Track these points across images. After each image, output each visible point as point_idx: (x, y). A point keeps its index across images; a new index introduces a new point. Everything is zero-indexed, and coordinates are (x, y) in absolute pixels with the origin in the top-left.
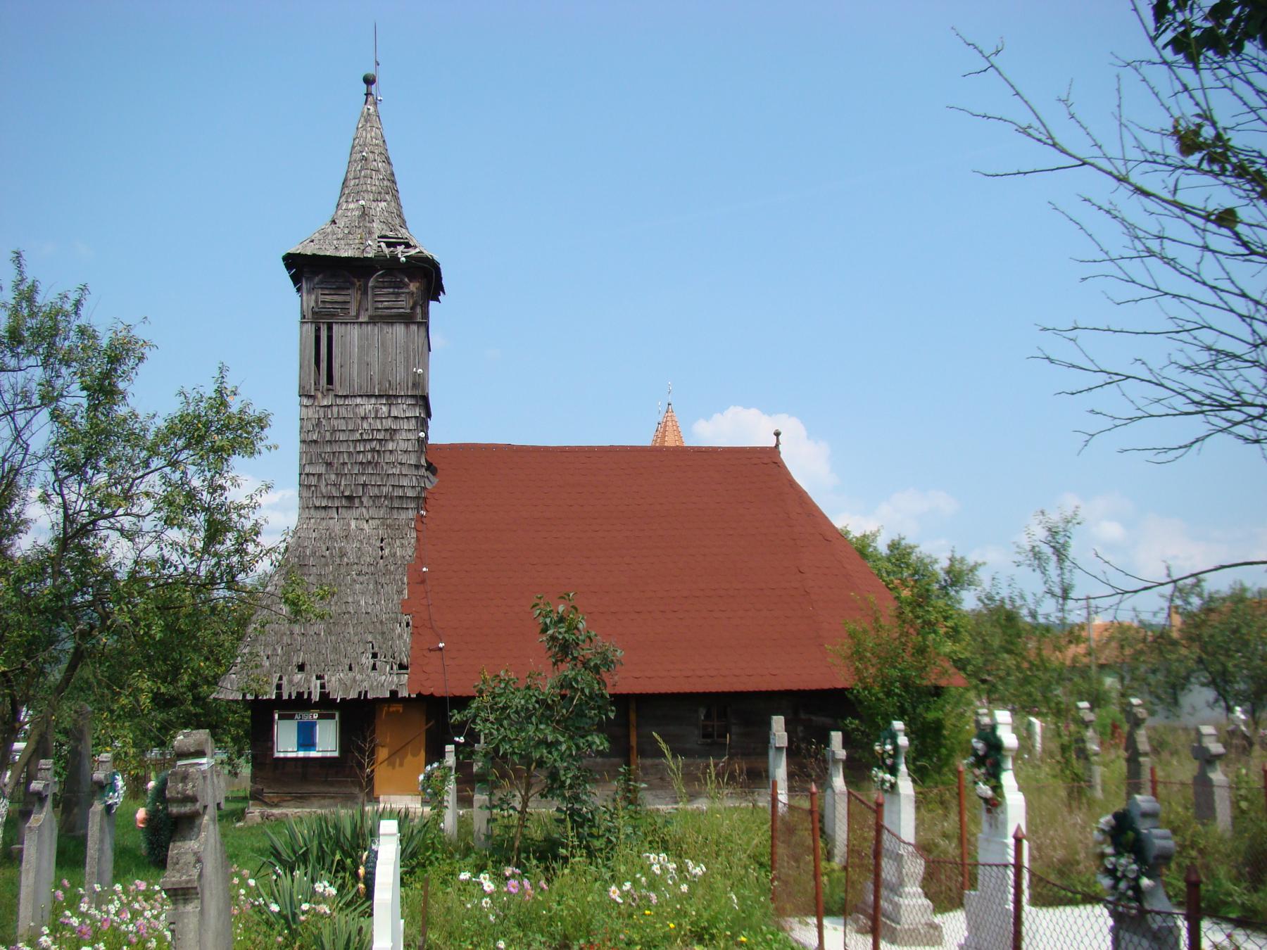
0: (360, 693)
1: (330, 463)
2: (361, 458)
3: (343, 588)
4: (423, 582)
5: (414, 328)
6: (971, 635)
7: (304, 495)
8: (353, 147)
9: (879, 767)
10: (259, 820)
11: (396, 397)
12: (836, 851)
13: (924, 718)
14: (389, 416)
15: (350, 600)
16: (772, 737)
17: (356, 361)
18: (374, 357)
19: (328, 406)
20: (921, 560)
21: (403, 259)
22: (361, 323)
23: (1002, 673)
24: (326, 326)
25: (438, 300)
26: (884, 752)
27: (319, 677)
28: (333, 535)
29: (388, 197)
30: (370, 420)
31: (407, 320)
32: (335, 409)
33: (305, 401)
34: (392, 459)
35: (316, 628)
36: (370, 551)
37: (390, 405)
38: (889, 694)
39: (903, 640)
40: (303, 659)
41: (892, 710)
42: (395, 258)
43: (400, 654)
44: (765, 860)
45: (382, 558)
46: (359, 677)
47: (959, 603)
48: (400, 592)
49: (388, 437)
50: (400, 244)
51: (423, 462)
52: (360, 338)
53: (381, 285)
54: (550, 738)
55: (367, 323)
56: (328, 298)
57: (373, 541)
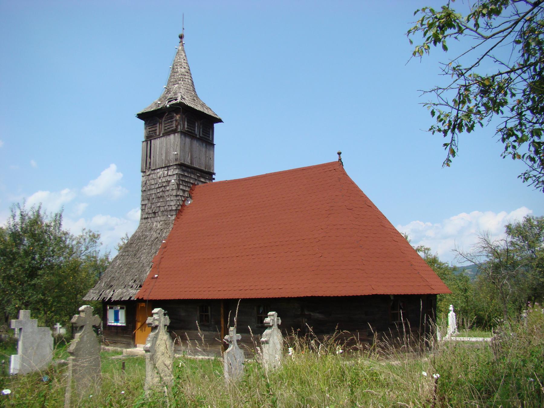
11: (170, 166)
30: (162, 178)
32: (151, 176)
56: (151, 130)
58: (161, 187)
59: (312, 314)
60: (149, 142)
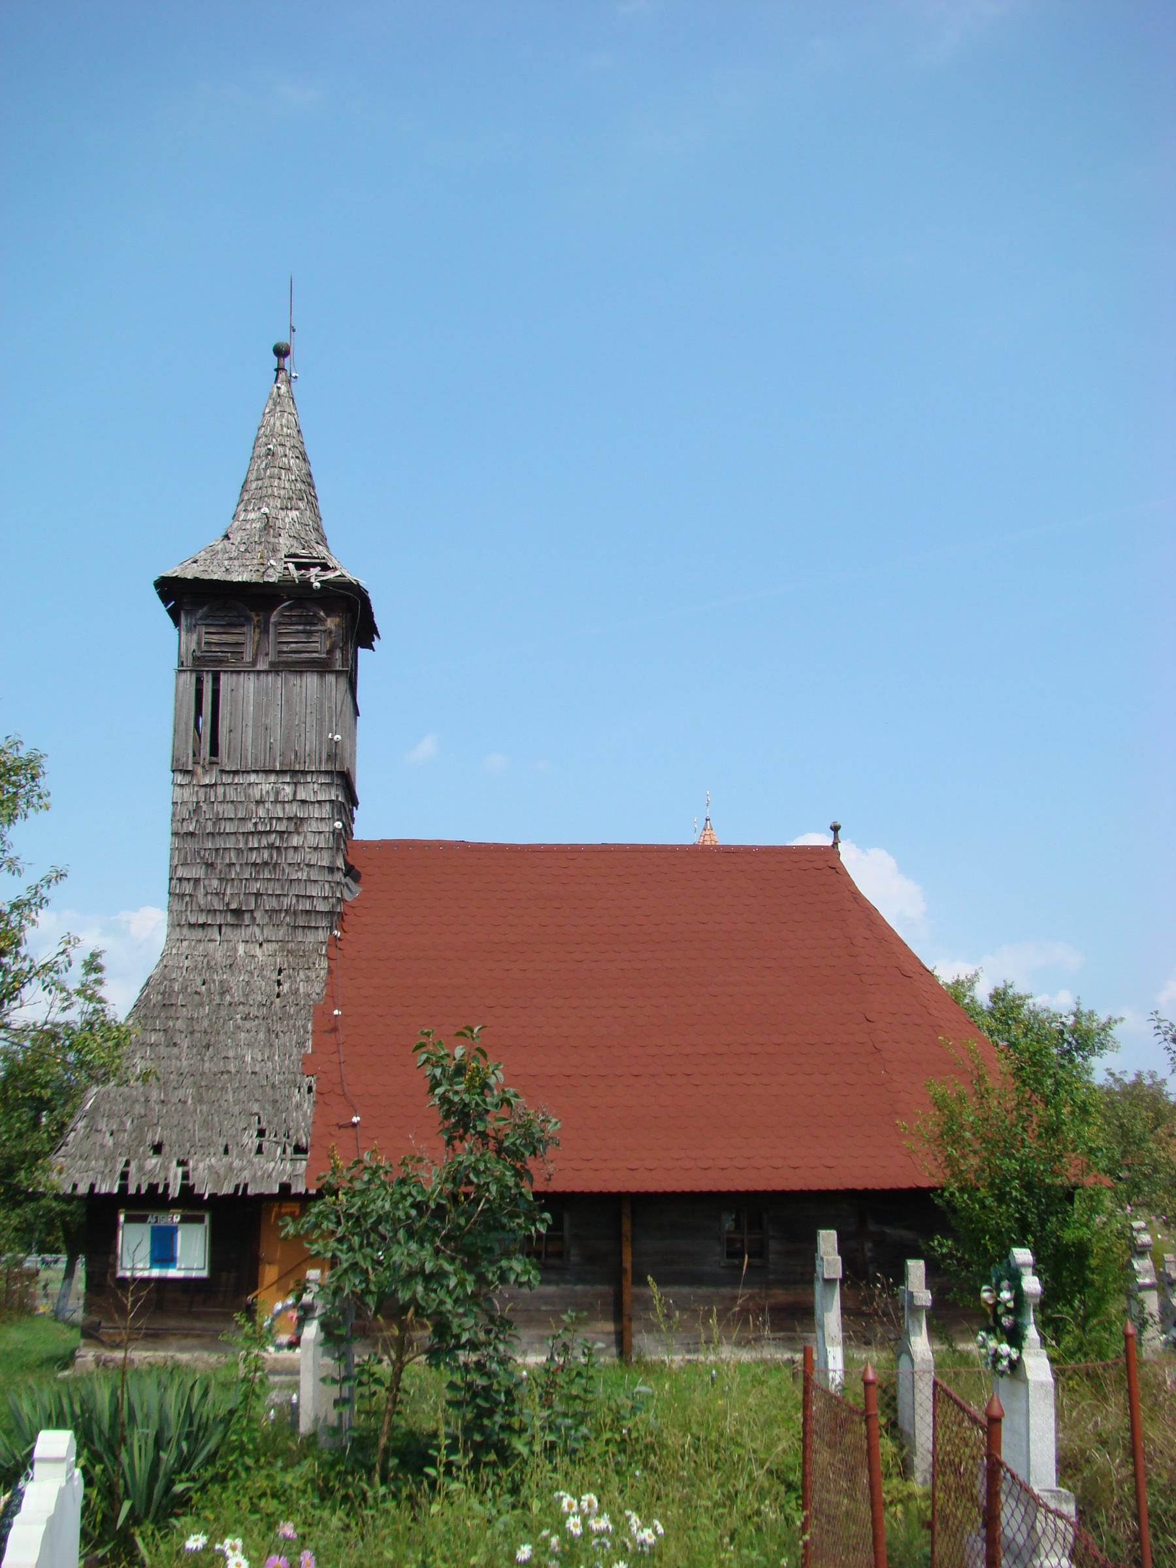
0: (237, 1187)
1: (212, 864)
2: (253, 857)
3: (222, 1037)
4: (334, 1030)
5: (331, 679)
6: (1104, 1116)
7: (175, 908)
8: (258, 438)
9: (989, 1330)
10: (92, 1366)
11: (304, 773)
12: (916, 1460)
13: (1058, 1238)
14: (294, 800)
15: (231, 1054)
16: (818, 1262)
17: (250, 723)
18: (276, 718)
19: (212, 786)
20: (1034, 1014)
21: (318, 585)
22: (259, 672)
23: (1147, 1170)
24: (210, 676)
25: (372, 648)
26: (998, 1303)
27: (181, 1163)
28: (213, 963)
29: (301, 505)
31: (321, 667)
32: (220, 790)
33: (180, 778)
35: (180, 1093)
36: (263, 986)
37: (296, 784)
38: (1001, 1198)
39: (1024, 1113)
40: (161, 1136)
41: (1007, 1224)
42: (307, 584)
43: (297, 1131)
44: (795, 1477)
45: (278, 996)
46: (237, 1163)
47: (1088, 1073)
48: (301, 1044)
49: (292, 828)
50: (314, 565)
51: (340, 863)
52: (257, 692)
53: (287, 620)
54: (429, 1267)
55: (267, 672)
56: (215, 638)
57: (267, 973)
59: (887, 1230)
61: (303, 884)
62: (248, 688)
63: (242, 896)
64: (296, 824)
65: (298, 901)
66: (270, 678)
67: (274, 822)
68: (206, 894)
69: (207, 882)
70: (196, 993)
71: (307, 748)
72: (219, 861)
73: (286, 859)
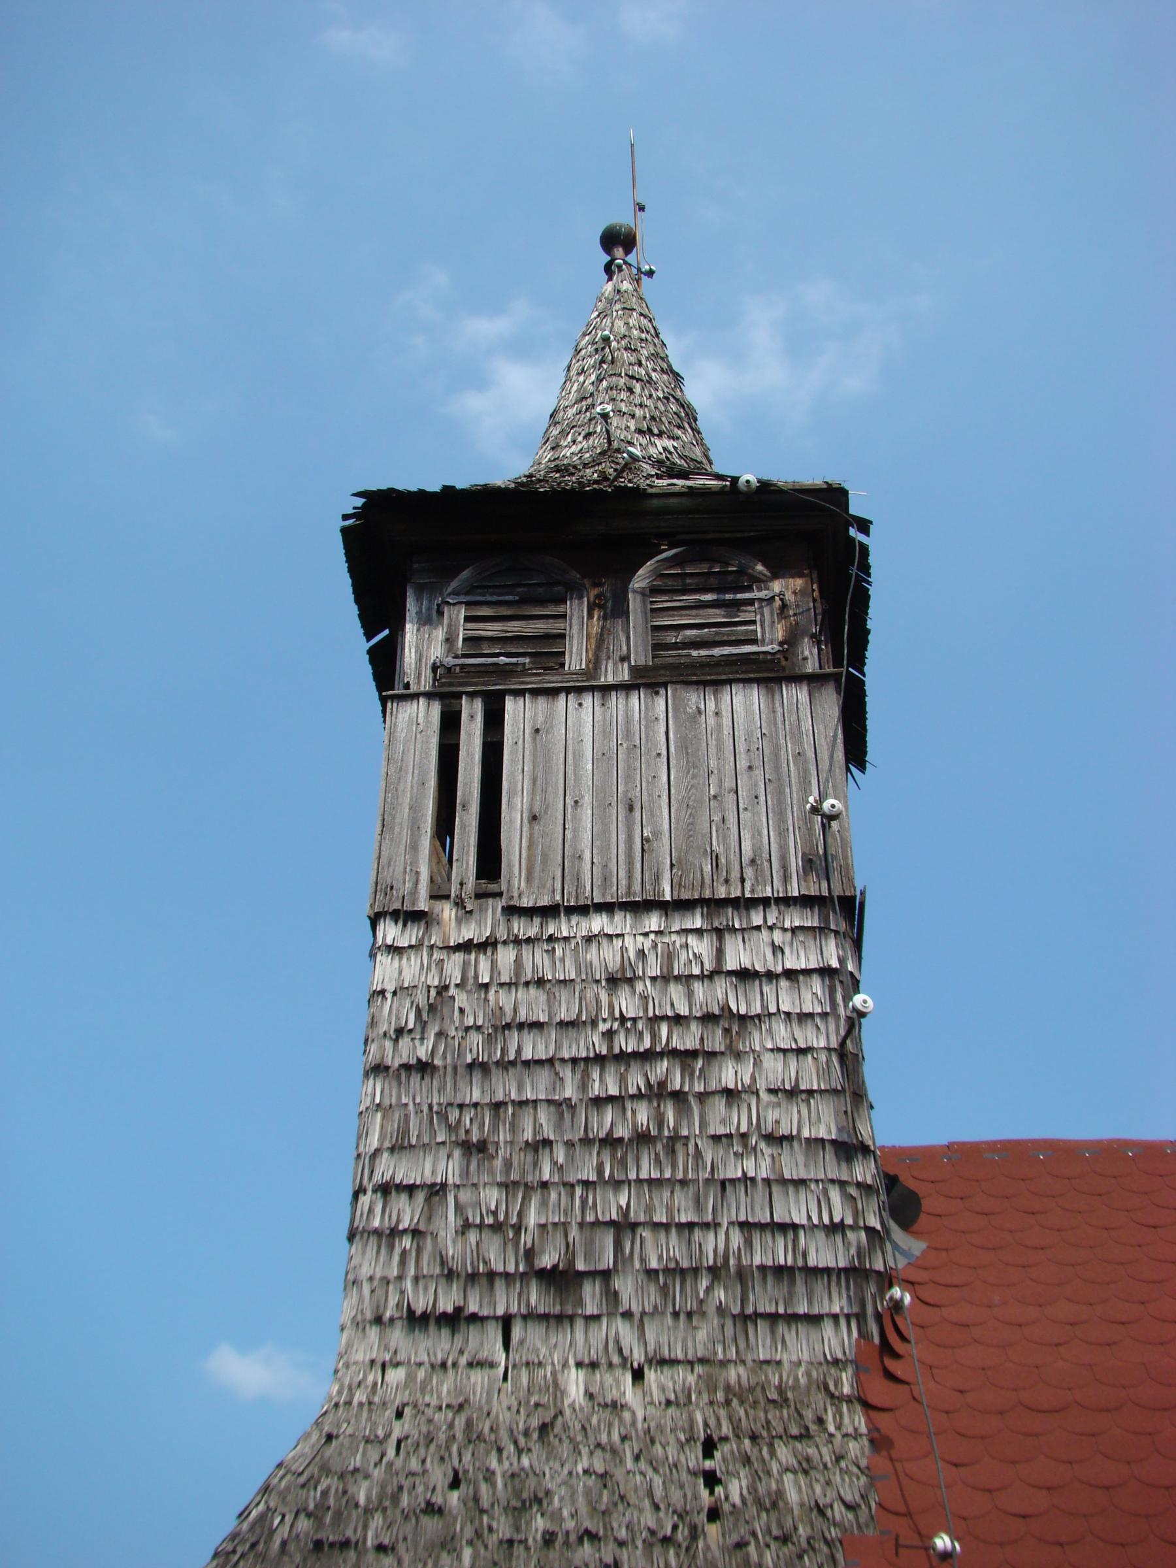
1: (482, 1147)
5: (799, 694)
14: (717, 972)
22: (606, 689)
24: (478, 705)
34: (740, 1119)
37: (719, 932)
45: (714, 1514)
49: (716, 1041)
53: (677, 584)
56: (491, 629)
58: (648, 1056)
60: (472, 716)
61: (760, 1191)
62: (579, 724)
63: (574, 1232)
64: (727, 1031)
65: (749, 1243)
66: (635, 701)
67: (664, 1029)
68: (466, 1226)
69: (465, 1196)
70: (432, 1509)
71: (747, 846)
72: (503, 1136)
73: (703, 1124)
